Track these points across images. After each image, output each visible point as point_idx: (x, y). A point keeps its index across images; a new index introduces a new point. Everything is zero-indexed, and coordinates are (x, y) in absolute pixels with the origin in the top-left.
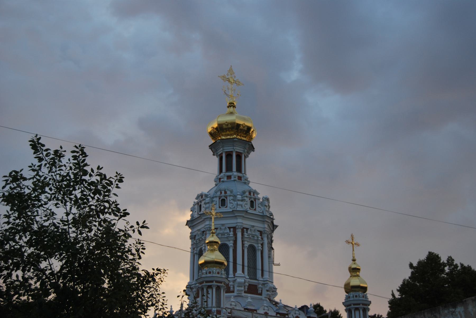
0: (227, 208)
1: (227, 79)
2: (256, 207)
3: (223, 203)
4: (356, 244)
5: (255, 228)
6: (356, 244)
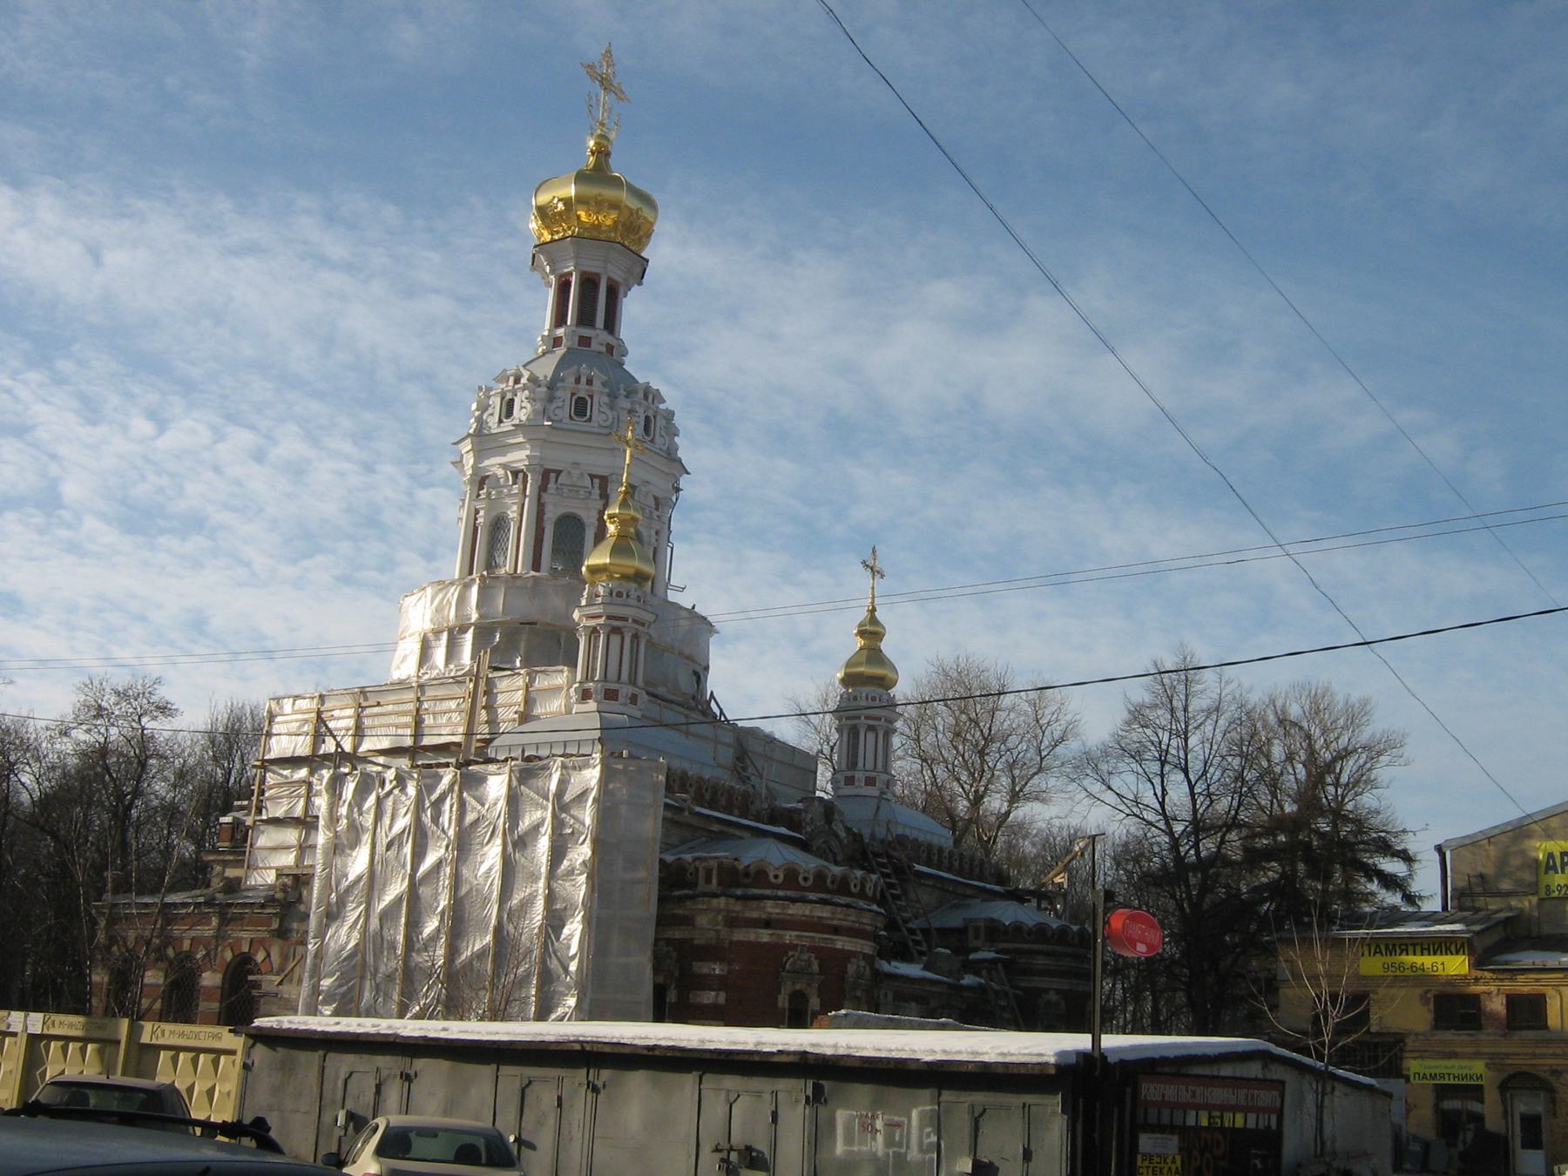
0: (592, 424)
2: (654, 434)
4: (878, 572)
6: (878, 572)
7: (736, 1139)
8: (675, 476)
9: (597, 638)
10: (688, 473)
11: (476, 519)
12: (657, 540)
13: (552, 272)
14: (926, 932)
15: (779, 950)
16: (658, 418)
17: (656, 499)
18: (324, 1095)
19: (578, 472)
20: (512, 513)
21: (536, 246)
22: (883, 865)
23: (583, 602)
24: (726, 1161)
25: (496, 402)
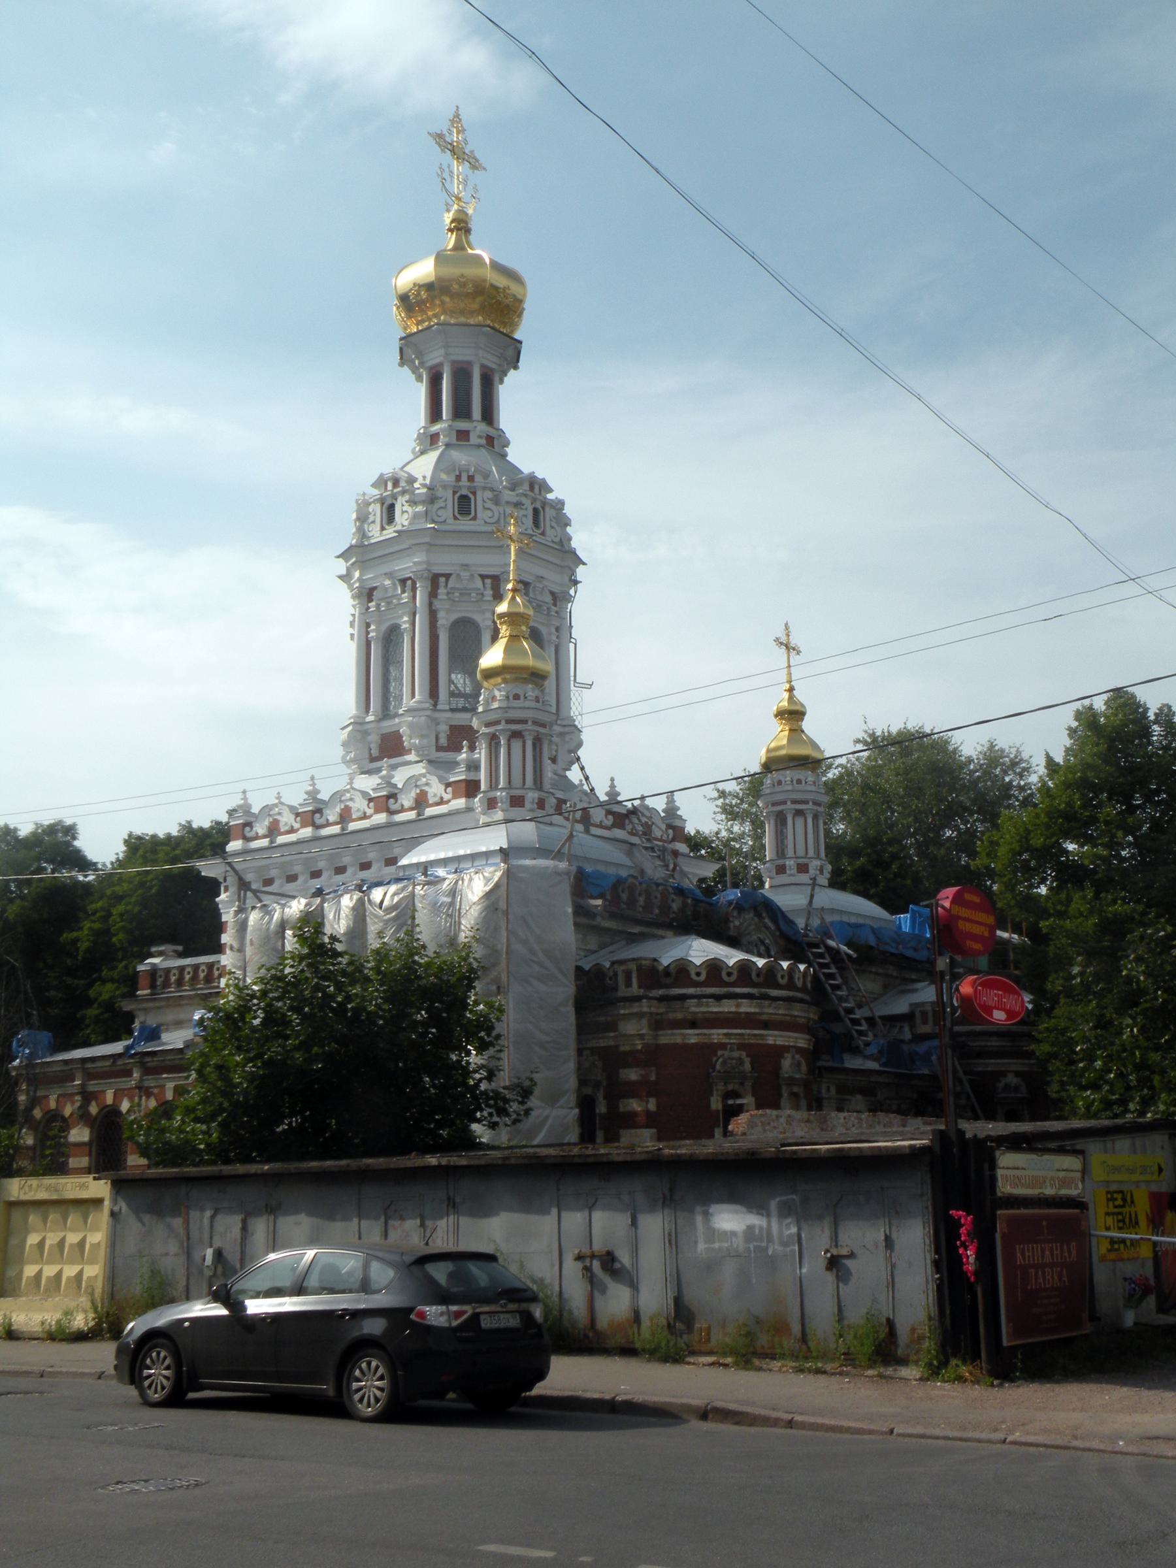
0: (477, 522)
1: (449, 146)
3: (464, 505)
4: (794, 649)
5: (545, 582)
7: (598, 1246)
8: (570, 568)
9: (498, 744)
10: (584, 564)
11: (368, 633)
12: (557, 637)
13: (422, 364)
14: (871, 1021)
15: (710, 1049)
16: (547, 509)
17: (553, 594)
18: (191, 1236)
19: (468, 574)
20: (404, 622)
21: (401, 339)
22: (821, 956)
23: (480, 709)
24: (588, 1269)
25: (376, 510)
